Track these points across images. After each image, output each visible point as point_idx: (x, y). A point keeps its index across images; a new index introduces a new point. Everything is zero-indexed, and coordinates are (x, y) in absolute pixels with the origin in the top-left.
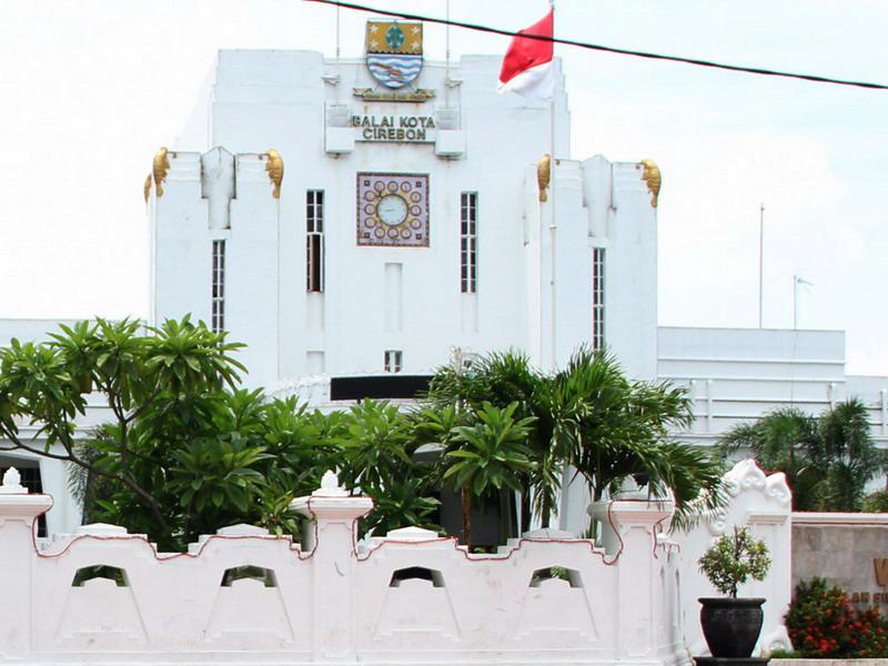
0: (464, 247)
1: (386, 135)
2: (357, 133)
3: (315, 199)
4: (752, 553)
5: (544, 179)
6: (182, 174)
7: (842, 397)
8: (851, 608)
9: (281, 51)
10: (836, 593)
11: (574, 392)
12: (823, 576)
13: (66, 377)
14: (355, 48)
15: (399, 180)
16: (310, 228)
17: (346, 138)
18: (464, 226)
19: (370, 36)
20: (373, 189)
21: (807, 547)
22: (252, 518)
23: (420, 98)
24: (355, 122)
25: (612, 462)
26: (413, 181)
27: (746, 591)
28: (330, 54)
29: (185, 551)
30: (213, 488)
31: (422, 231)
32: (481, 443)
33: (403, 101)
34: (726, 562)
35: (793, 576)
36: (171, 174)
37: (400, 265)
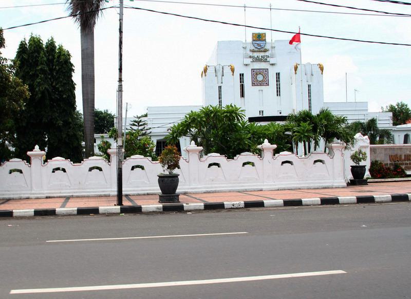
0: (277, 85)
1: (258, 60)
2: (251, 60)
3: (242, 75)
4: (362, 155)
5: (296, 68)
6: (210, 71)
7: (370, 118)
8: (384, 167)
9: (233, 41)
10: (381, 163)
11: (321, 118)
12: (377, 159)
13: (204, 119)
14: (250, 40)
15: (261, 70)
16: (241, 82)
17: (248, 61)
18: (277, 80)
19: (253, 36)
20: (255, 73)
21: (373, 153)
22: (249, 151)
23: (265, 51)
24: (250, 57)
25: (330, 136)
26: (265, 70)
27: (362, 163)
28: (244, 41)
29: (233, 159)
30: (239, 144)
31: (267, 82)
32: (301, 131)
33: (261, 52)
34: (357, 157)
35: (371, 160)
36: (208, 71)
37: (262, 90)
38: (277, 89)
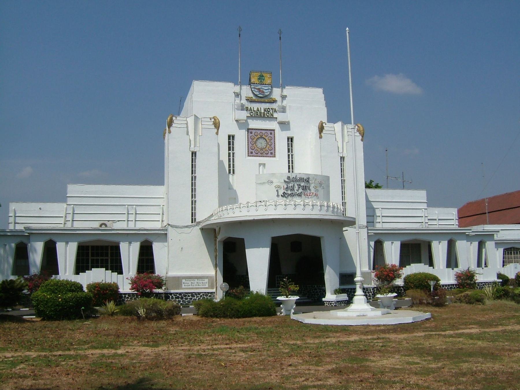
0: (289, 158)
3: (231, 138)
18: (289, 149)
38: (289, 163)
